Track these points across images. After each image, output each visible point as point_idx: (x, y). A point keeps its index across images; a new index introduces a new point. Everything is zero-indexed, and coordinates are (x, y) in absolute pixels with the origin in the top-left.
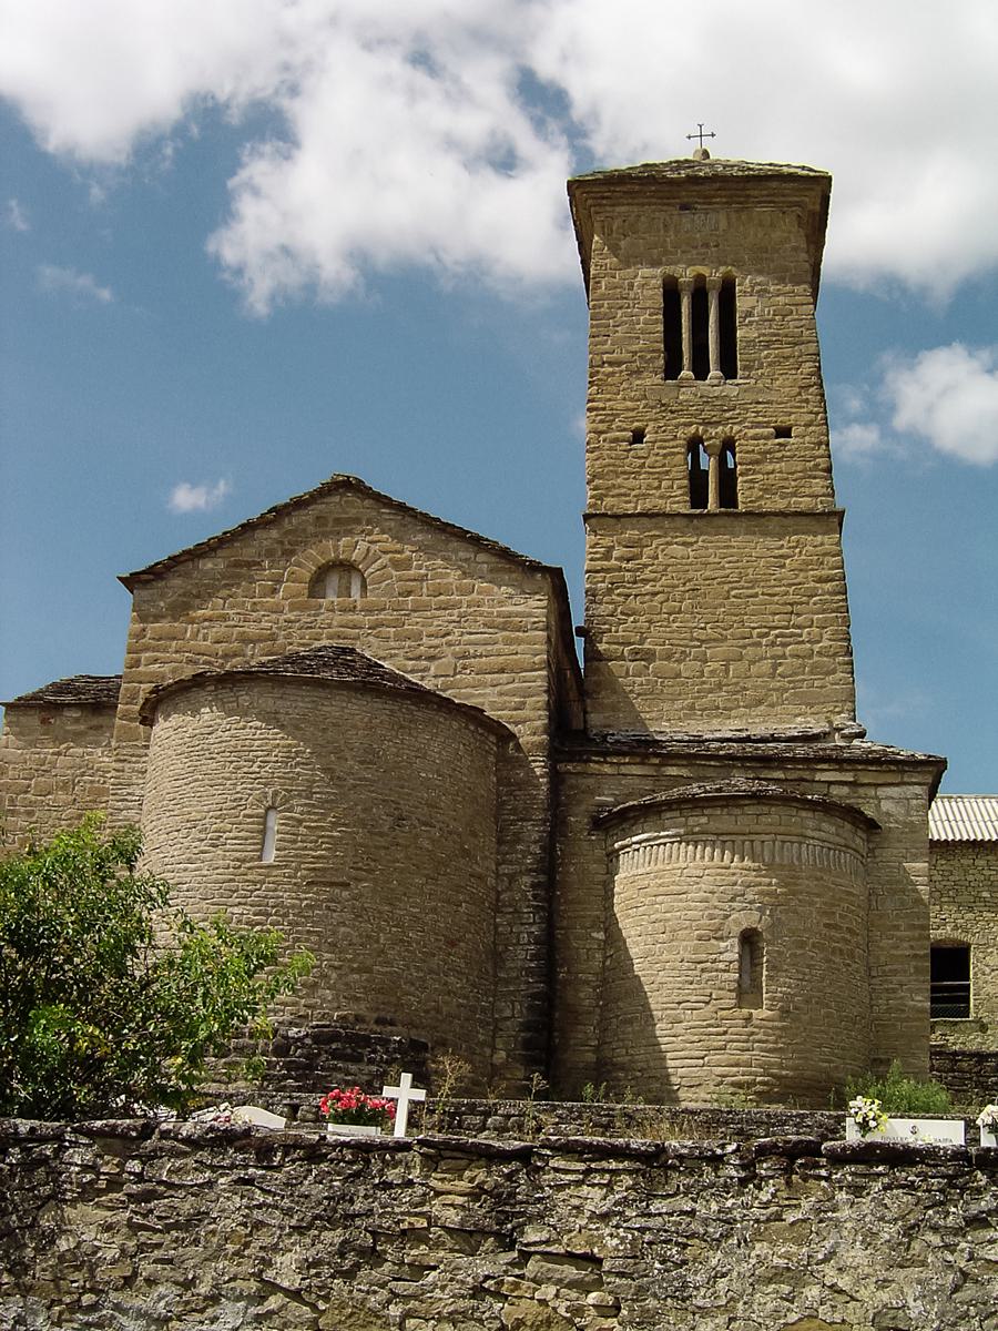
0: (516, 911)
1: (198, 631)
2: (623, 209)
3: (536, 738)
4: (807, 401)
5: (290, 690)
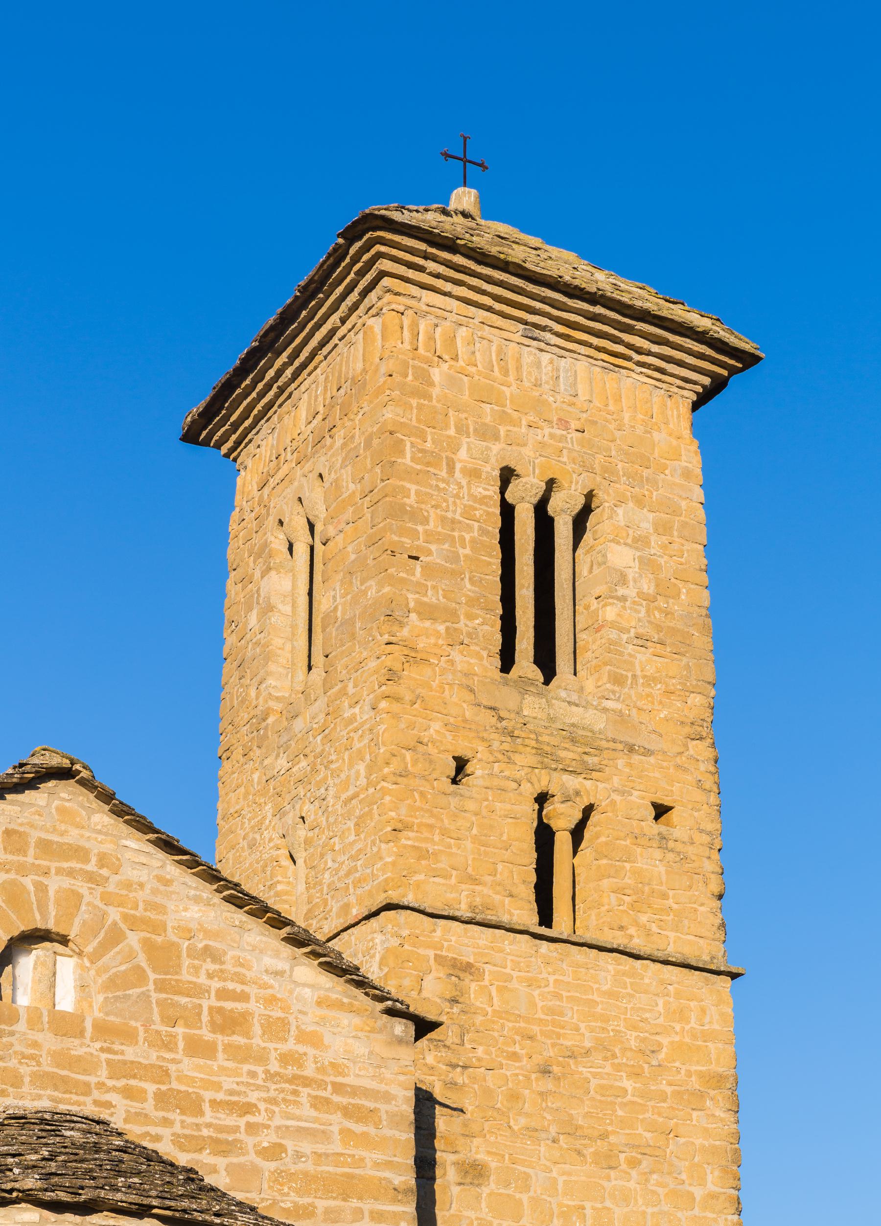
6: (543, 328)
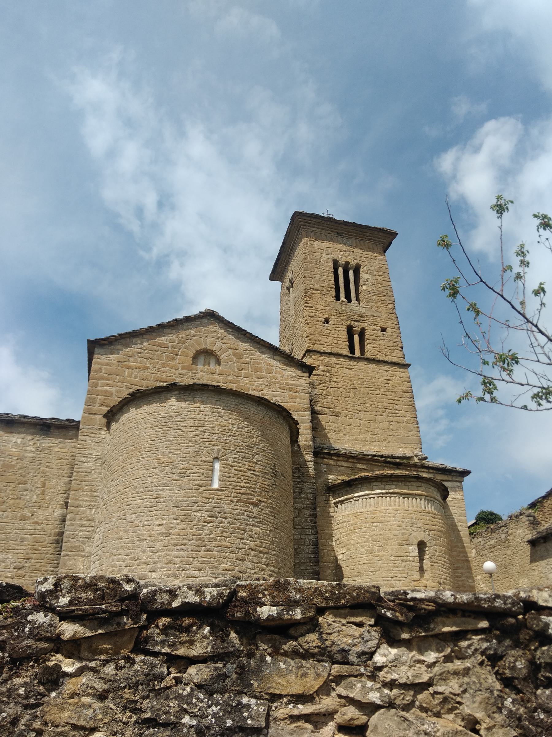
1: (132, 373)
2: (315, 229)
3: (307, 443)
4: (391, 319)
5: (224, 398)
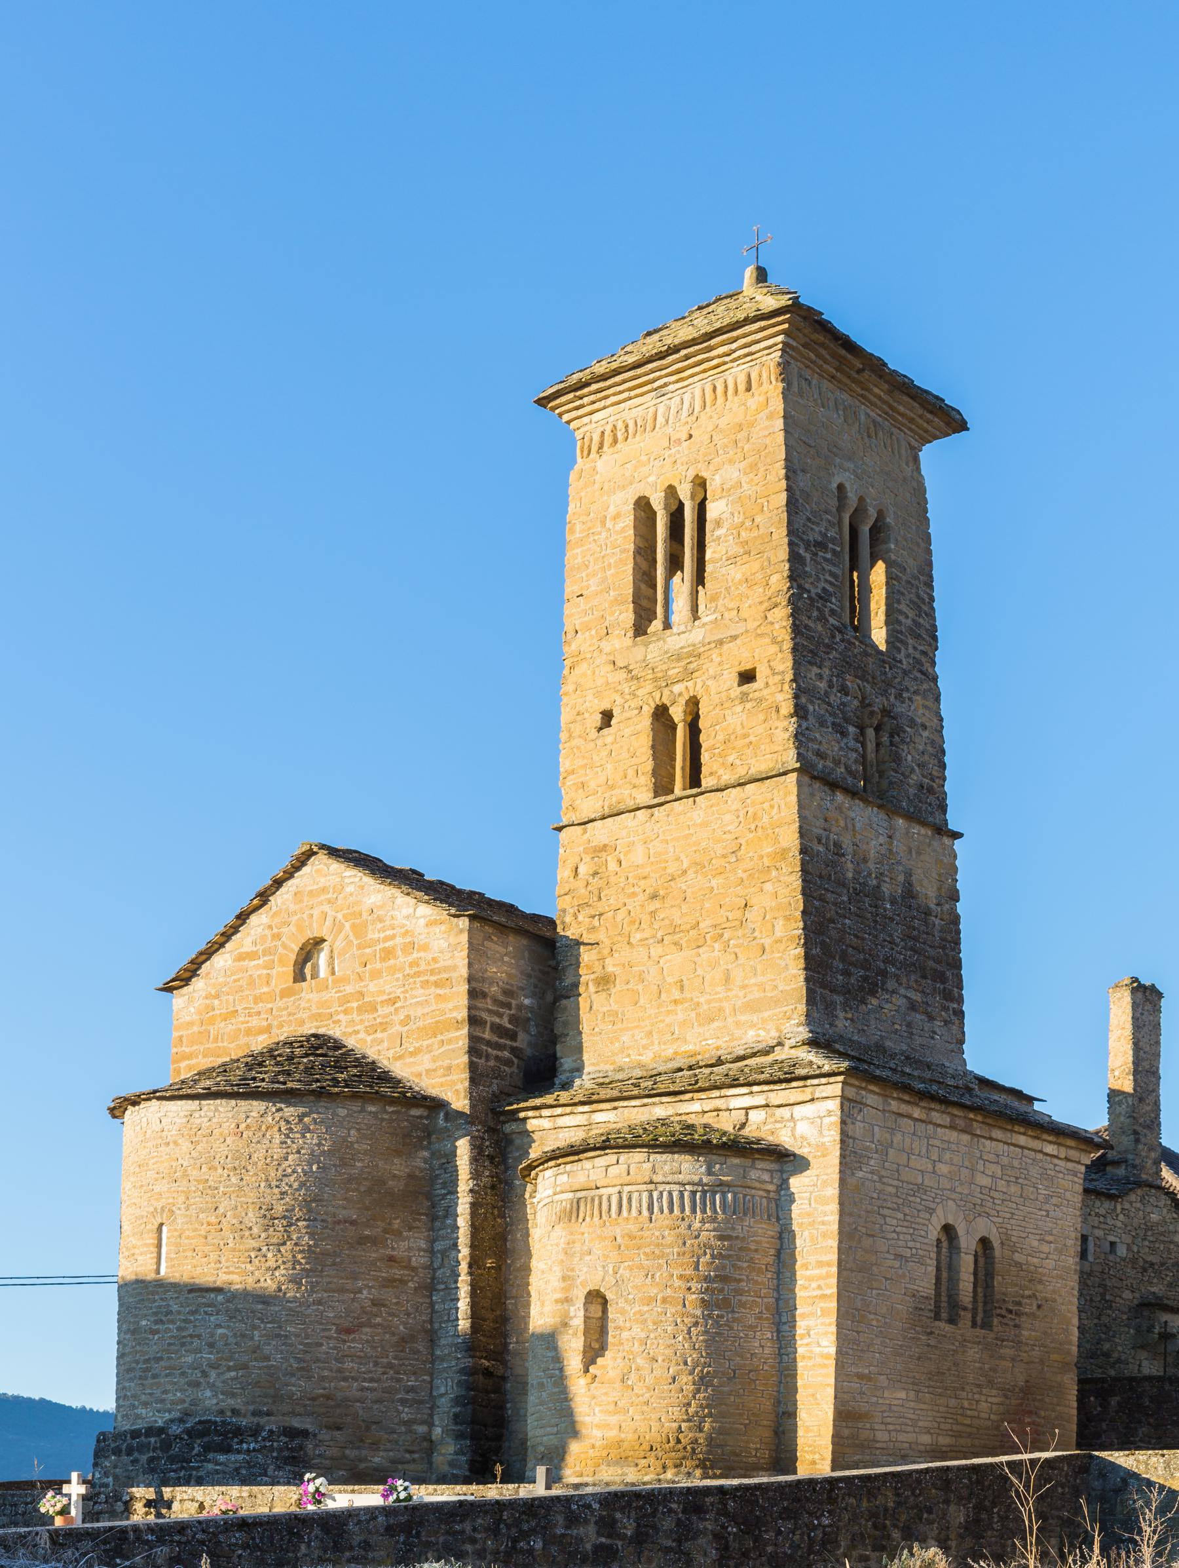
0: (446, 1288)
6: (665, 385)
